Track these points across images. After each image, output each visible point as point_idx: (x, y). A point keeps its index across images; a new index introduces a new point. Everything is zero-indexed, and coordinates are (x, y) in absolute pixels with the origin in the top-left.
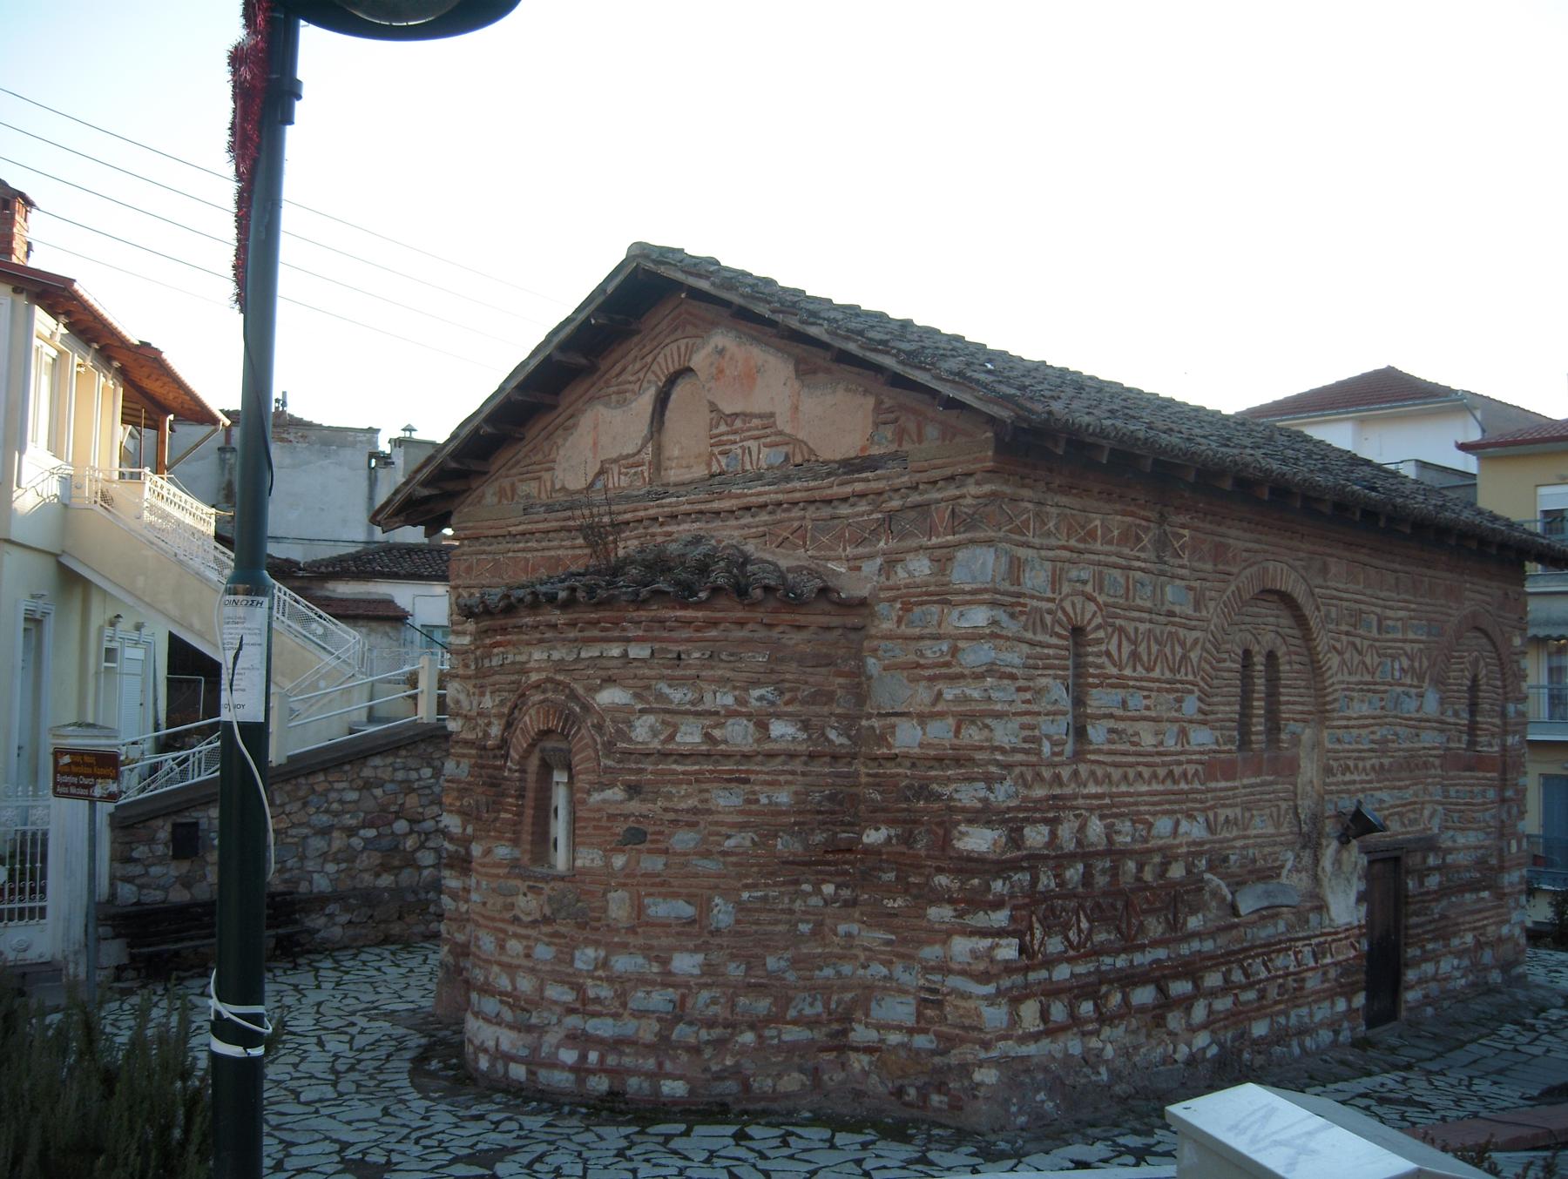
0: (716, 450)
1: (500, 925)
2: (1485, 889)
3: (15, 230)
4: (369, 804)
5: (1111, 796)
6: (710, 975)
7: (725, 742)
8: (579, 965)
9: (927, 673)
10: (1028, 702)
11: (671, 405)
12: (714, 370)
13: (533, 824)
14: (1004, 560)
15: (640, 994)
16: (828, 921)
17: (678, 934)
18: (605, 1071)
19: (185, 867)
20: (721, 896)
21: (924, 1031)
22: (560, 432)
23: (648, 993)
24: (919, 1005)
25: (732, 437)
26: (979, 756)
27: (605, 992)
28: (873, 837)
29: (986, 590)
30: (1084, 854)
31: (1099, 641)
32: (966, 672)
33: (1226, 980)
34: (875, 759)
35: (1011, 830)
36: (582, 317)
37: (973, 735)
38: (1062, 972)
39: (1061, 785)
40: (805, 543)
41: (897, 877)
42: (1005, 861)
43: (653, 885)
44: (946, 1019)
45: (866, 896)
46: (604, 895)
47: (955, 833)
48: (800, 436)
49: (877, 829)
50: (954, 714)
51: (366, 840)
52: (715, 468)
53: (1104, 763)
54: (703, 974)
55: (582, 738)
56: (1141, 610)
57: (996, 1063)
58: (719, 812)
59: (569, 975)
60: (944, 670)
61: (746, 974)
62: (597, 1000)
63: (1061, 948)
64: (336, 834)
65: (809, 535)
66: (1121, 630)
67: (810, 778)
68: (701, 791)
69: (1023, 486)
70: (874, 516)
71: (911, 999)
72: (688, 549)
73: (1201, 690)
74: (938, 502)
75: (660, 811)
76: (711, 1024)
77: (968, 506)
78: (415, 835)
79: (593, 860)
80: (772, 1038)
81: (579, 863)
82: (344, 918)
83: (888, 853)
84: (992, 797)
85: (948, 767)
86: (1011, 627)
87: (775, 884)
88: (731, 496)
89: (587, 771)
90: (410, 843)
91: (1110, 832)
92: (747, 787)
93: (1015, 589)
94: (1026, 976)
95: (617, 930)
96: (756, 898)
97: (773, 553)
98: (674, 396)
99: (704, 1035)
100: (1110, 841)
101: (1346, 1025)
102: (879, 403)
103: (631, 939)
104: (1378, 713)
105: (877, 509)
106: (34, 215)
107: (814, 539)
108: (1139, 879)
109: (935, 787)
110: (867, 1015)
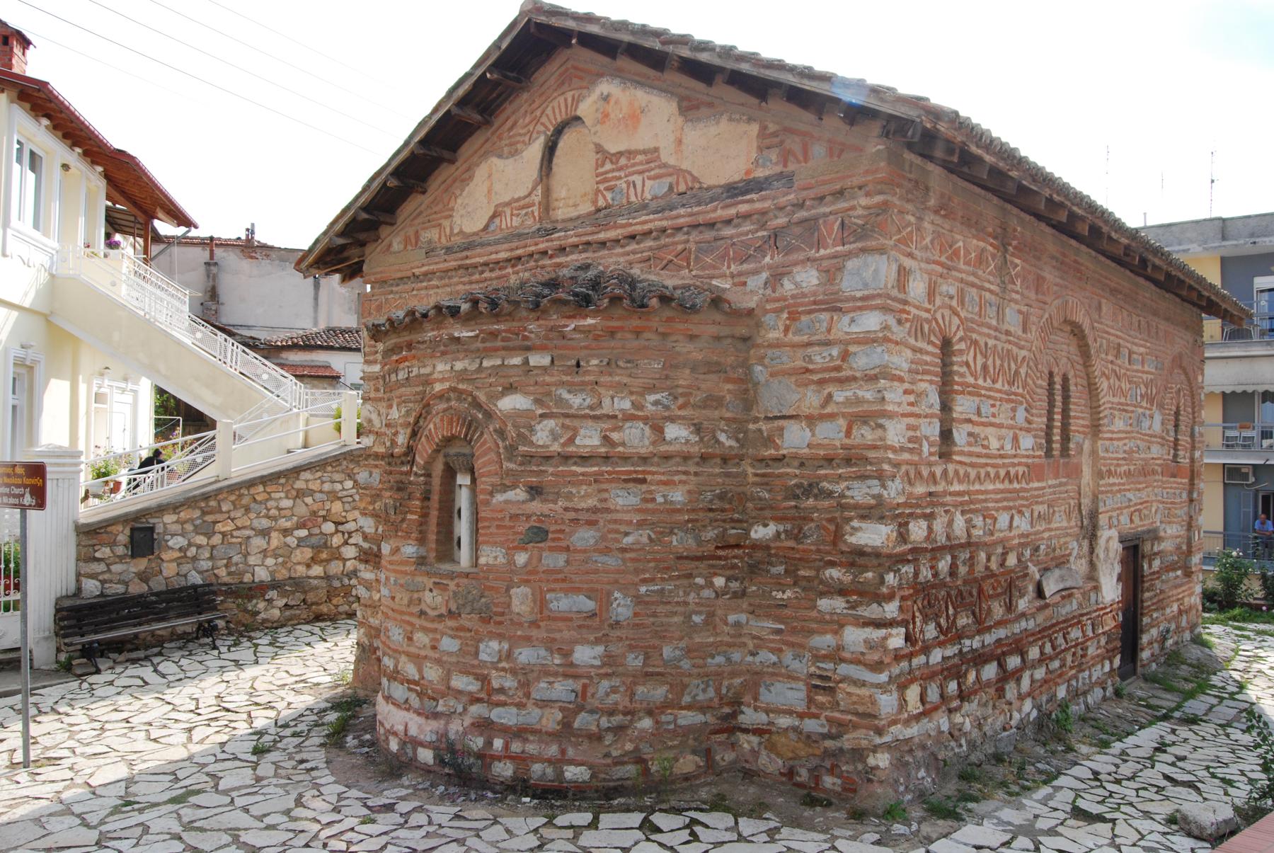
0: (602, 187)
1: (407, 618)
2: (1179, 568)
3: (14, 61)
4: (302, 510)
5: (968, 493)
6: (610, 665)
7: (623, 444)
8: (483, 657)
9: (815, 377)
10: (911, 404)
11: (558, 152)
12: (600, 116)
13: (438, 524)
14: (894, 267)
15: (543, 685)
16: (719, 612)
17: (580, 627)
18: (510, 758)
19: (142, 564)
20: (620, 590)
21: (816, 716)
22: (457, 184)
23: (550, 683)
24: (809, 691)
25: (616, 174)
26: (871, 454)
27: (510, 683)
28: (760, 533)
29: (879, 296)
30: (952, 548)
31: (961, 352)
32: (858, 375)
33: (1042, 653)
34: (761, 460)
35: (900, 525)
36: (479, 72)
37: (866, 434)
38: (936, 656)
39: (935, 483)
40: (689, 264)
41: (786, 571)
42: (896, 555)
43: (556, 581)
44: (838, 704)
45: (754, 588)
46: (508, 590)
47: (848, 528)
48: (684, 167)
49: (766, 525)
50: (844, 415)
51: (300, 539)
52: (601, 203)
53: (965, 464)
54: (604, 665)
55: (485, 442)
56: (989, 327)
57: (887, 747)
58: (617, 511)
59: (473, 666)
60: (834, 374)
61: (645, 664)
62: (501, 690)
63: (935, 634)
64: (274, 534)
65: (693, 256)
66: (976, 343)
67: (700, 478)
68: (600, 491)
69: (908, 201)
70: (760, 234)
71: (801, 685)
72: (579, 273)
73: (1027, 402)
74: (825, 215)
75: (561, 511)
76: (611, 713)
77: (858, 217)
78: (340, 535)
79: (496, 558)
80: (669, 723)
81: (482, 561)
82: (281, 602)
83: (778, 548)
84: (885, 493)
85: (839, 466)
86: (899, 332)
87: (671, 578)
88: (616, 227)
89: (489, 474)
90: (337, 541)
91: (970, 525)
92: (644, 487)
93: (901, 296)
94: (910, 661)
95: (520, 624)
96: (652, 591)
97: (658, 274)
98: (561, 145)
99: (604, 722)
100: (969, 535)
101: (1109, 682)
102: (763, 128)
103: (534, 633)
104: (1129, 428)
105: (763, 226)
106: (30, 52)
107: (697, 259)
108: (987, 568)
109: (825, 484)
110: (756, 699)
